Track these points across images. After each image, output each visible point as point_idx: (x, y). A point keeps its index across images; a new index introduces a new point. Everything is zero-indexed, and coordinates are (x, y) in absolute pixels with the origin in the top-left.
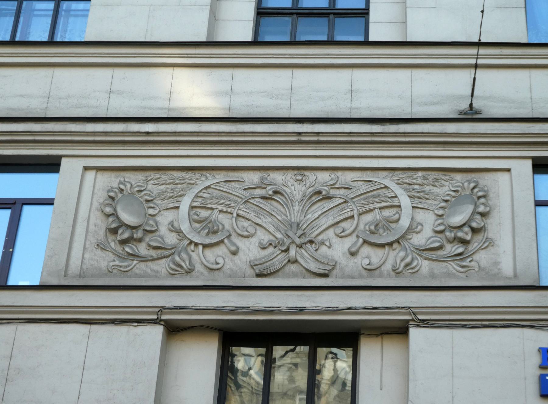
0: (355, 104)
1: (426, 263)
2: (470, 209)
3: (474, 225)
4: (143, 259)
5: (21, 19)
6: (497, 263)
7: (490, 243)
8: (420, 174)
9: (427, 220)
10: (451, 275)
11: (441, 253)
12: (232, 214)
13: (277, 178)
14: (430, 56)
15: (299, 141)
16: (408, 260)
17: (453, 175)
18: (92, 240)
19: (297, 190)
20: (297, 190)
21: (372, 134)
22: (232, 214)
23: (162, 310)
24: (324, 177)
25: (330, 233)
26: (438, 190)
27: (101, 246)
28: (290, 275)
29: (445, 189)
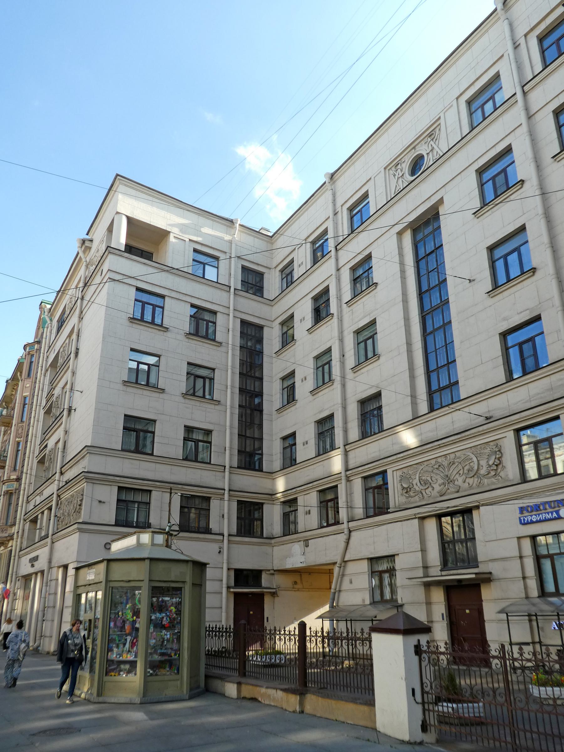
0: (455, 427)
1: (486, 480)
2: (494, 457)
3: (495, 463)
4: (412, 497)
5: (440, 376)
6: (507, 475)
7: (504, 467)
8: (479, 447)
9: (483, 463)
10: (494, 483)
11: (490, 475)
12: (245, 577)
13: (439, 460)
14: (472, 401)
15: (440, 447)
16: (479, 481)
17: (489, 443)
18: (400, 493)
19: (446, 463)
20: (446, 463)
21: (459, 438)
22: (245, 577)
23: (415, 515)
24: (452, 456)
25: (457, 476)
26: (486, 451)
27: (402, 495)
28: (449, 494)
29: (487, 451)
